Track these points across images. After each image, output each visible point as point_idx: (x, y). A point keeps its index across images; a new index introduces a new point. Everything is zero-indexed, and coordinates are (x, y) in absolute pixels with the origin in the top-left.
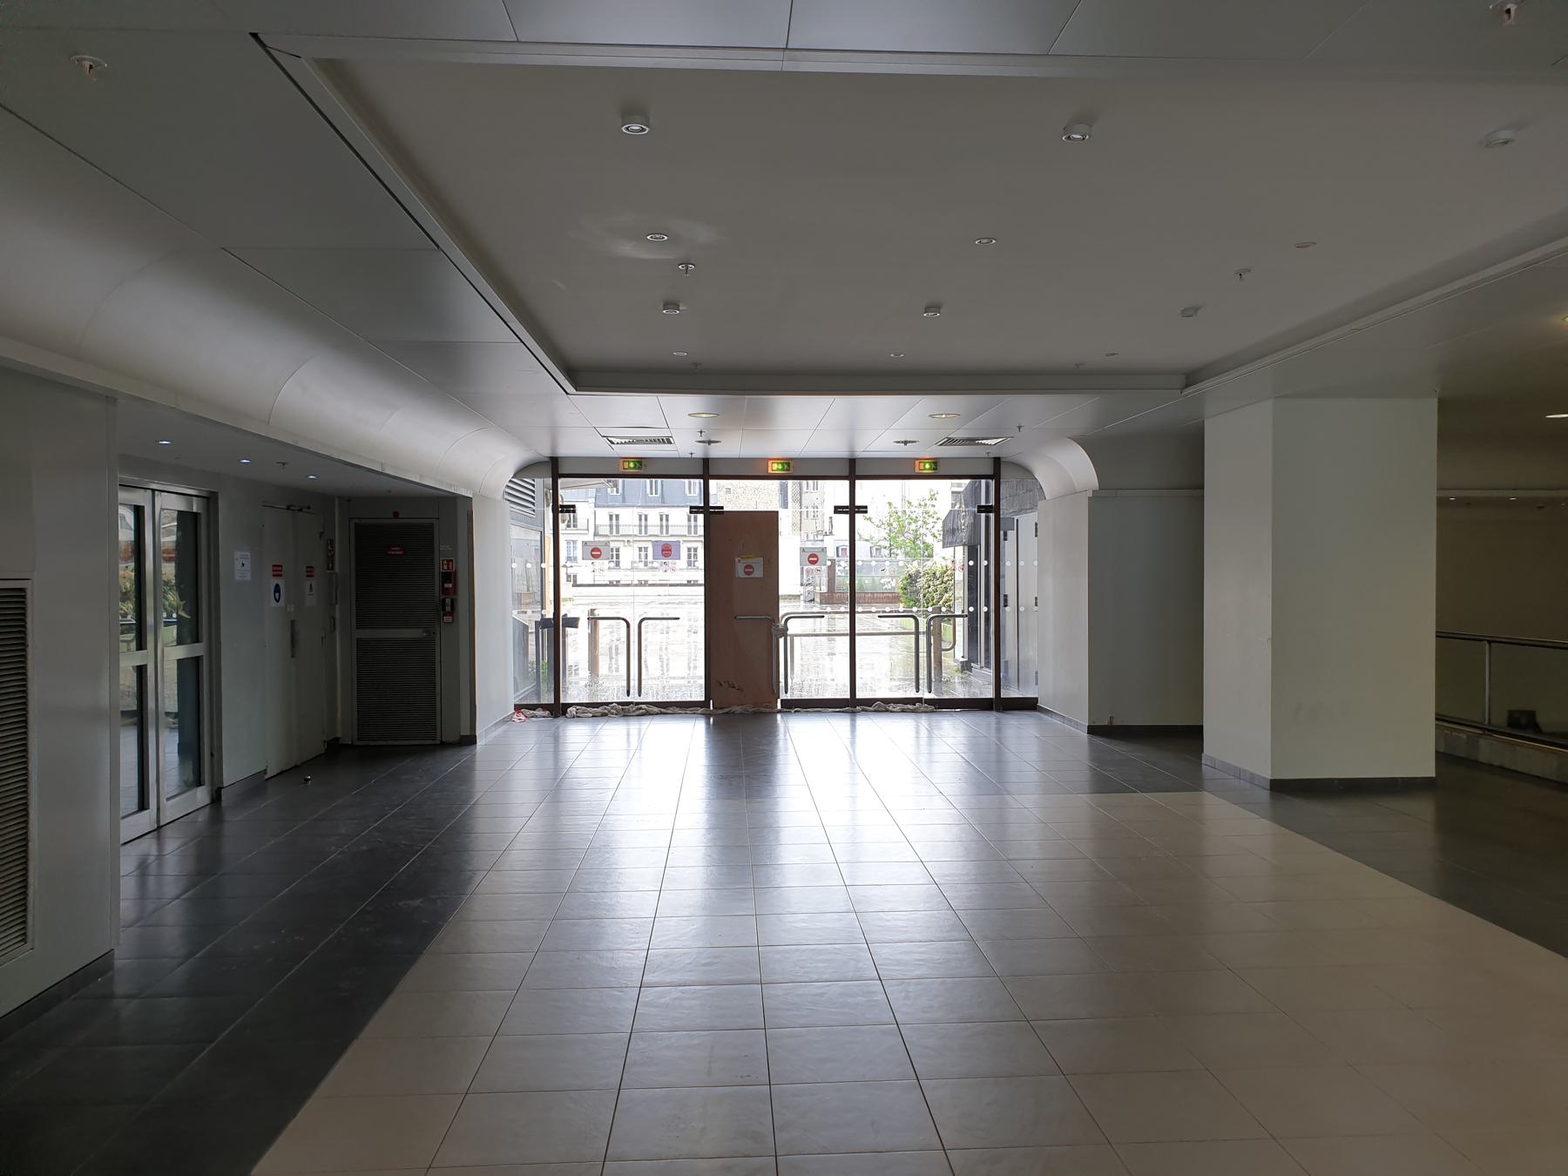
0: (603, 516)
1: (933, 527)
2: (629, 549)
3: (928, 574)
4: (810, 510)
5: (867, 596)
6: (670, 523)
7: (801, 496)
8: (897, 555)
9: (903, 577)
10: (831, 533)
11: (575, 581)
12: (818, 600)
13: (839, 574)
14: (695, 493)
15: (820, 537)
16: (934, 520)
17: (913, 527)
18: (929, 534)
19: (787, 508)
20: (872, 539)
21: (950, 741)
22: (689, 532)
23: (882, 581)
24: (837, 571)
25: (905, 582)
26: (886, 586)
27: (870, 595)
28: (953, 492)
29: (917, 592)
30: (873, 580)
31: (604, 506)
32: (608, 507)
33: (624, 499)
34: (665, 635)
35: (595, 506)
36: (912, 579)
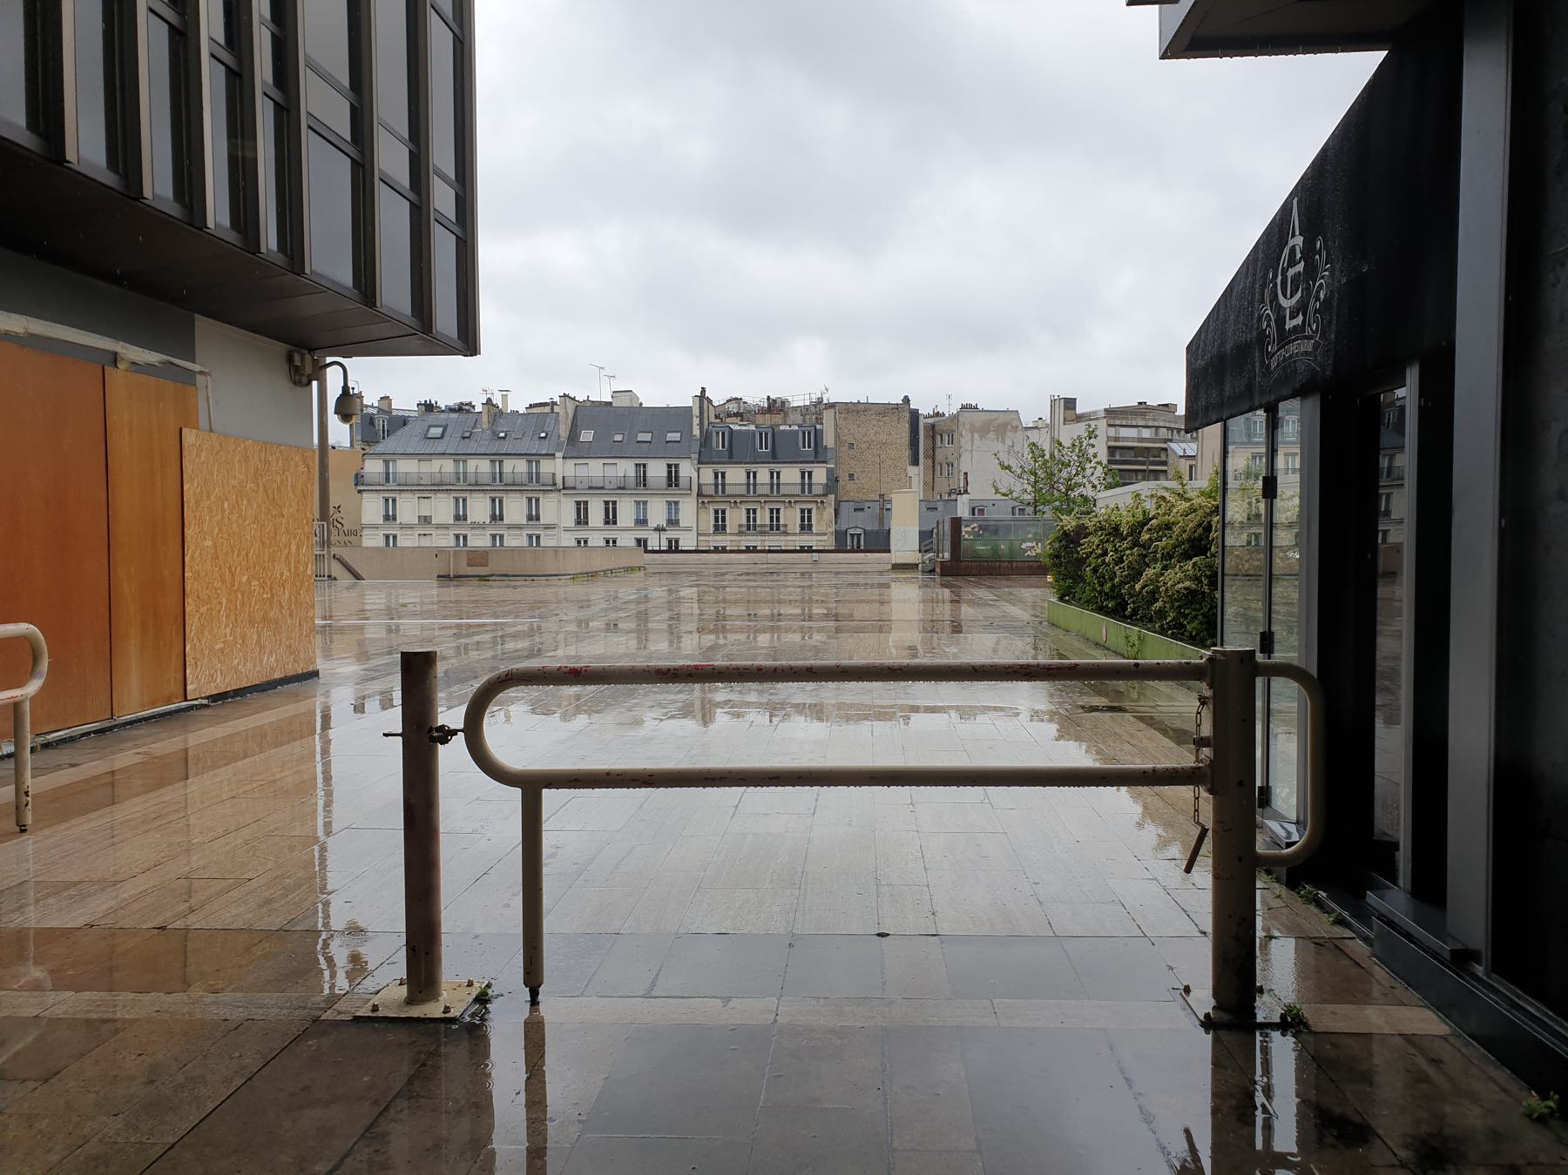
0: (707, 475)
1: (1093, 474)
2: (736, 511)
3: (1102, 529)
4: (945, 467)
5: (1002, 564)
6: (782, 481)
7: (934, 451)
8: (1044, 513)
9: (1052, 536)
10: (966, 492)
11: (646, 546)
12: (938, 570)
13: (967, 536)
14: (809, 447)
15: (953, 497)
16: (1093, 464)
17: (1064, 474)
18: (1089, 486)
19: (918, 464)
20: (1011, 493)
21: (1225, 1018)
22: (803, 491)
23: (1024, 546)
24: (963, 533)
25: (1057, 545)
26: (1029, 553)
27: (1006, 564)
28: (1109, 447)
29: (1081, 562)
30: (1012, 544)
31: (708, 463)
32: (713, 463)
33: (731, 455)
34: (752, 613)
35: (699, 463)
36: (1070, 540)
